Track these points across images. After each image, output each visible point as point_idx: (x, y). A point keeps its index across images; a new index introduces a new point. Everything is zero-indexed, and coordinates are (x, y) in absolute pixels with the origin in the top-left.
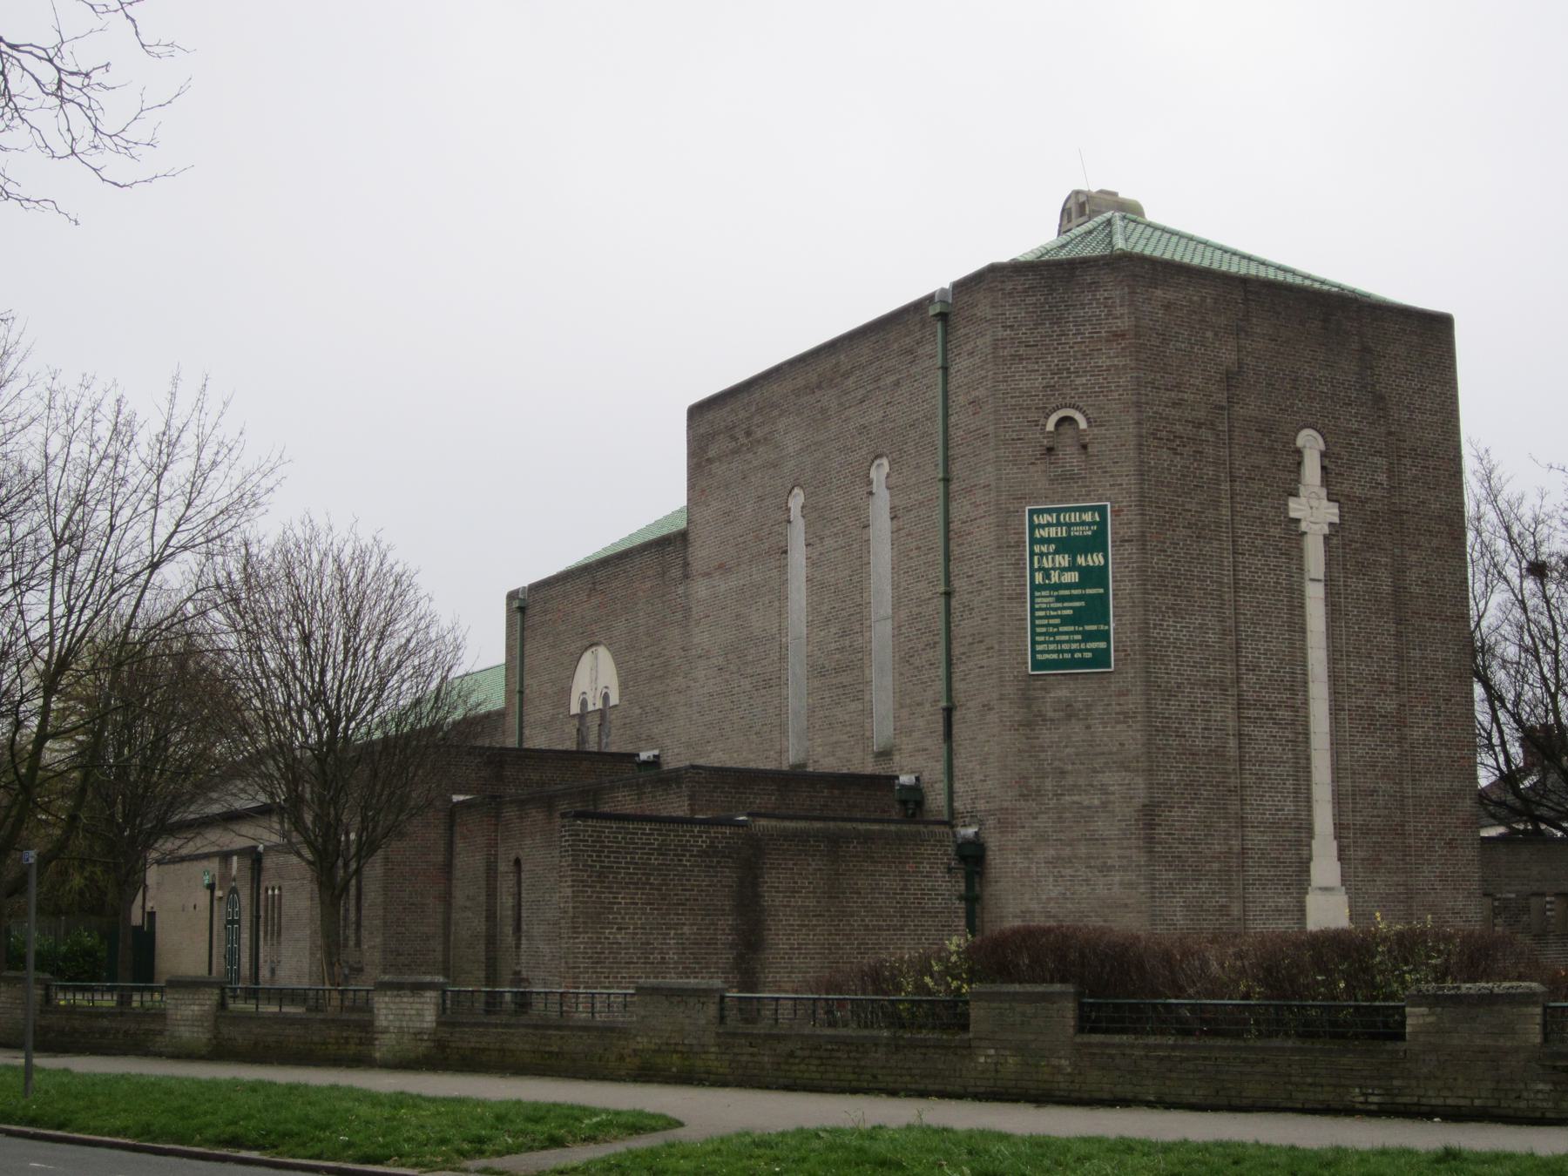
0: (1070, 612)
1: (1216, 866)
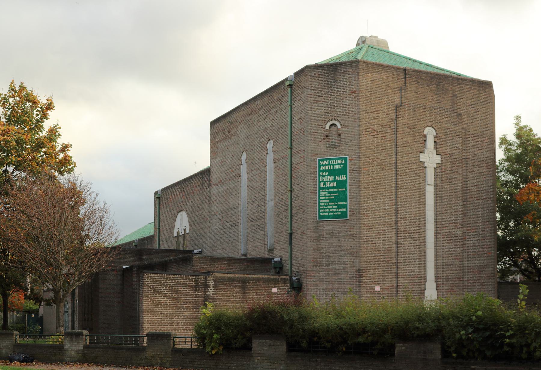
0: (333, 197)
1: (387, 292)
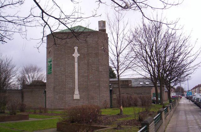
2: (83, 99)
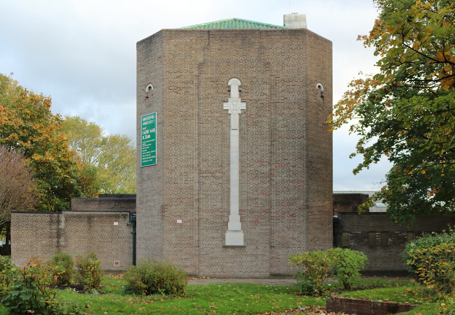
0: (148, 147)
2: (254, 247)
